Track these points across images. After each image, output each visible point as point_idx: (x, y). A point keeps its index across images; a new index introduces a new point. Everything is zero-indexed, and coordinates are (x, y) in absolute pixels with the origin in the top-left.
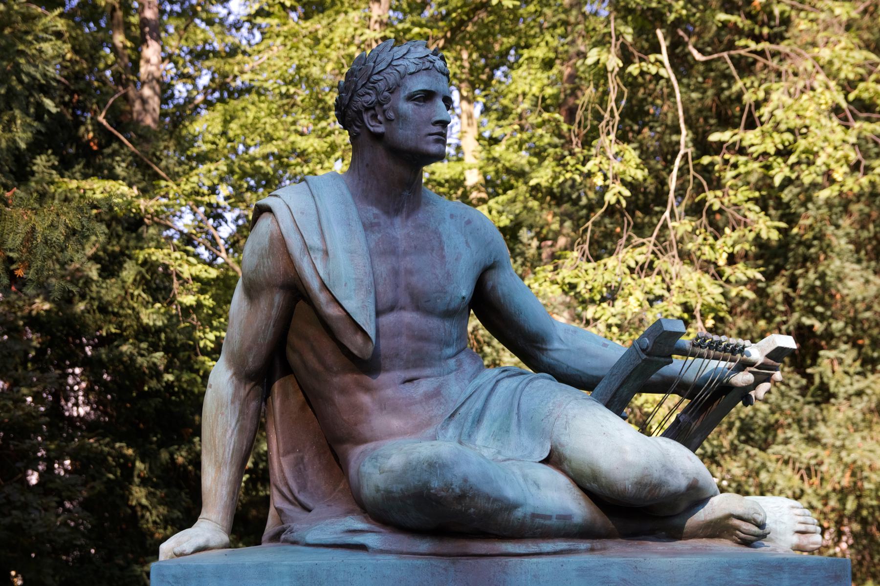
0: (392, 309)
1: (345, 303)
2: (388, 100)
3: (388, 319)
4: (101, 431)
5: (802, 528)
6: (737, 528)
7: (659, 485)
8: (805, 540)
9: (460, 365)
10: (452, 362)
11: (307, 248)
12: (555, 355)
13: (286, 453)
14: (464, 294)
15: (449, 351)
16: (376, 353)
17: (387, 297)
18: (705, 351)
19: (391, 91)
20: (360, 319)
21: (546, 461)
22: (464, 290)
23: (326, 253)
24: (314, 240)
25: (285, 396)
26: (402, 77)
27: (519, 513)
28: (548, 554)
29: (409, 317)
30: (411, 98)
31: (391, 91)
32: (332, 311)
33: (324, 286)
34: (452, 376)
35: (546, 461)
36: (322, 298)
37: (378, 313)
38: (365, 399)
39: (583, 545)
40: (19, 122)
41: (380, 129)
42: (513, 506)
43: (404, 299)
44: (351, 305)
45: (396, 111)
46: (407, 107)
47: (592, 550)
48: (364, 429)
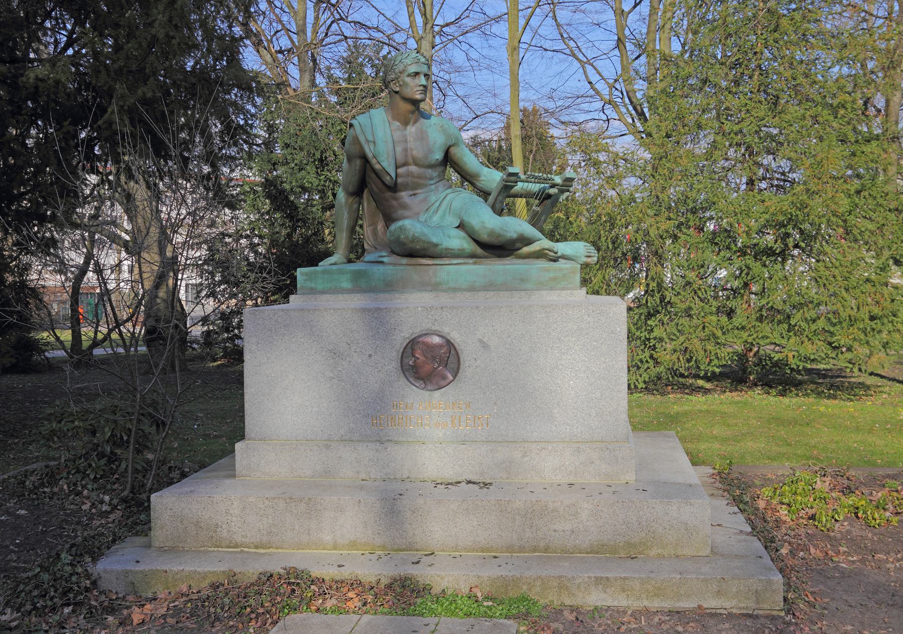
0: (405, 164)
1: (382, 164)
2: (399, 77)
3: (400, 171)
4: (543, 218)
5: (589, 254)
6: (547, 254)
7: (499, 236)
8: (589, 260)
9: (437, 188)
10: (433, 187)
11: (368, 141)
12: (483, 182)
13: (370, 226)
14: (437, 157)
15: (432, 182)
16: (396, 183)
17: (401, 159)
18: (533, 180)
19: (401, 73)
20: (388, 170)
21: (458, 227)
22: (439, 156)
23: (374, 142)
24: (370, 138)
25: (369, 201)
26: (405, 67)
27: (440, 247)
28: (457, 264)
29: (413, 169)
30: (409, 75)
31: (401, 73)
32: (377, 167)
33: (374, 157)
34: (432, 193)
35: (458, 227)
36: (374, 161)
37: (397, 167)
38: (394, 203)
39: (471, 261)
40: (153, 472)
41: (398, 89)
42: (436, 245)
43: (411, 160)
44: (385, 164)
45: (403, 82)
46: (408, 80)
47: (475, 263)
48: (394, 216)
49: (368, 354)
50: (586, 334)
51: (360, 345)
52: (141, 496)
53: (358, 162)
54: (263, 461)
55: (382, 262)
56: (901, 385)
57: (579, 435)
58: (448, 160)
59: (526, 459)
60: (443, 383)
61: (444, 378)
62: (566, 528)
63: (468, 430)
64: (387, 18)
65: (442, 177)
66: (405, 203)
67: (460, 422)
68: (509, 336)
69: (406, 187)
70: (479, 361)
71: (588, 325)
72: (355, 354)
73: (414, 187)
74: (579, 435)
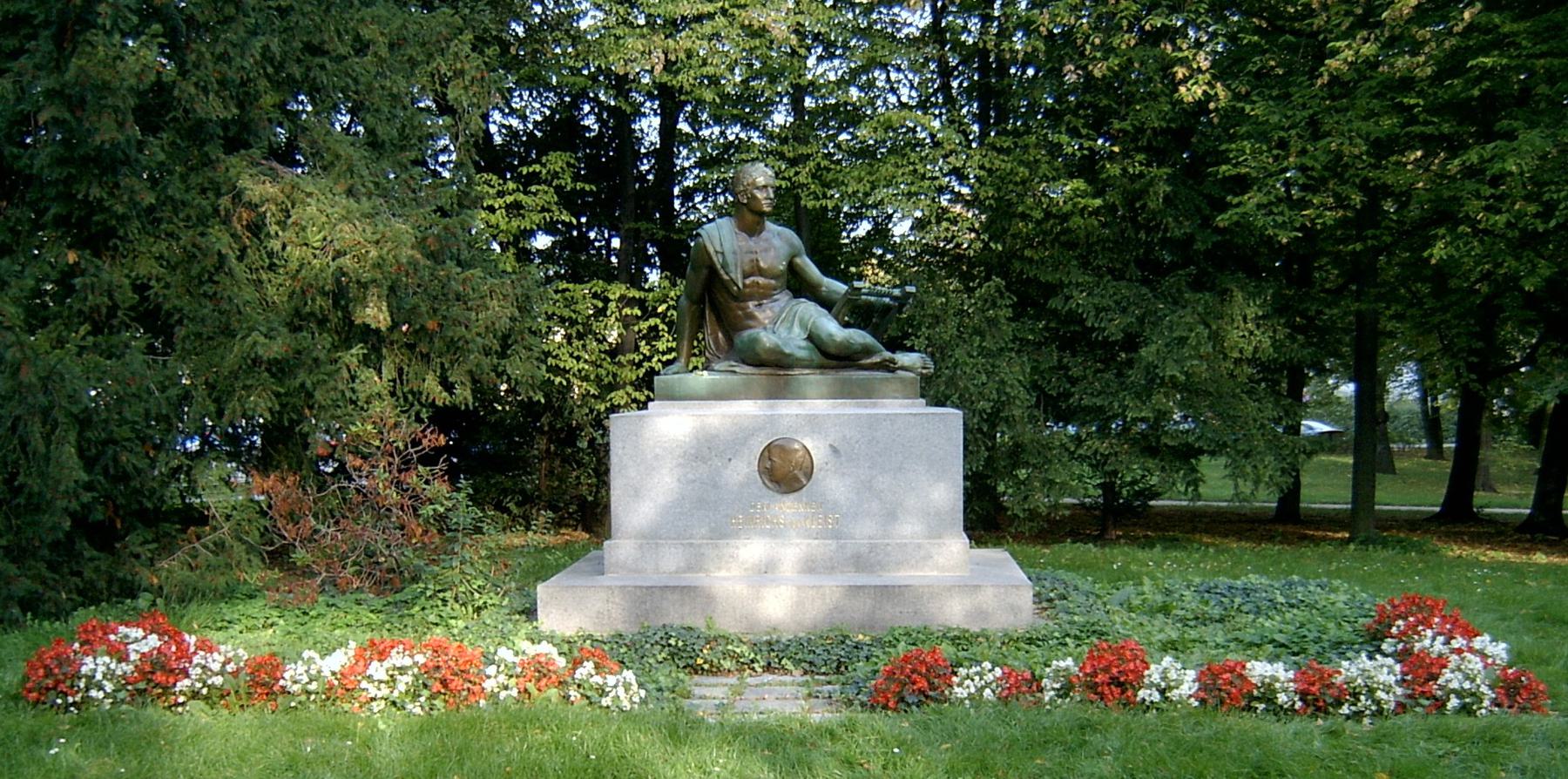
11: (717, 252)
23: (723, 253)
24: (719, 249)
55: (734, 372)
60: (797, 485)
73: (764, 295)
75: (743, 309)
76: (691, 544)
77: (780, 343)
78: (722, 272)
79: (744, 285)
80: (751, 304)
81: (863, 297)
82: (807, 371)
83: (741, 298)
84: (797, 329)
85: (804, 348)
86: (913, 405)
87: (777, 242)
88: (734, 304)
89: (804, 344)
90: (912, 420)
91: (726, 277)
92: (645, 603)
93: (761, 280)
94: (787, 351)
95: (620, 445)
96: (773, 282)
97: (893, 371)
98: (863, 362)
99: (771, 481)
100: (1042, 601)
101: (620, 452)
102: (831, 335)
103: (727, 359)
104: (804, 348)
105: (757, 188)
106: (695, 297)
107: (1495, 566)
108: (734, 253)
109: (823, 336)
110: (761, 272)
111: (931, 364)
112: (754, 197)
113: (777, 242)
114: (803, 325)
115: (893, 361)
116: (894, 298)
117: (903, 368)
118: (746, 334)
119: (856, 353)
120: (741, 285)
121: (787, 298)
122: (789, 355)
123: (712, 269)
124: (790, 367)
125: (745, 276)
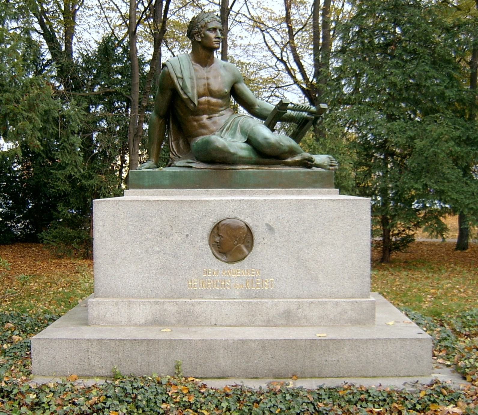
11: (177, 77)
23: (182, 79)
24: (179, 75)
44: (190, 95)
45: (204, 34)
49: (186, 234)
50: (342, 220)
51: (180, 227)
52: (435, 207)
53: (169, 94)
54: (108, 313)
55: (191, 167)
56: (236, 2)
57: (336, 293)
58: (234, 92)
59: (300, 310)
60: (240, 256)
61: (241, 251)
62: (334, 359)
63: (257, 290)
64: (265, 42)
65: (228, 105)
66: (204, 123)
67: (252, 284)
68: (288, 222)
69: (204, 112)
70: (266, 240)
71: (343, 214)
72: (176, 234)
73: (211, 110)
74: (336, 293)
75: (197, 121)
76: (157, 302)
77: (226, 144)
78: (181, 92)
79: (199, 103)
80: (205, 117)
81: (289, 112)
82: (247, 167)
83: (197, 112)
84: (238, 134)
85: (244, 149)
86: (329, 193)
87: (223, 72)
88: (191, 117)
89: (245, 145)
90: (331, 204)
91: (185, 97)
92: (118, 353)
93: (213, 100)
94: (232, 150)
95: (101, 223)
96: (220, 101)
97: (310, 167)
98: (289, 160)
99: (220, 252)
100: (87, 60)
101: (101, 229)
102: (266, 139)
103: (186, 158)
104: (244, 149)
105: (209, 30)
106: (162, 113)
107: (304, 173)
108: (191, 78)
109: (260, 139)
110: (211, 93)
111: (335, 162)
112: (207, 37)
113: (223, 72)
114: (244, 132)
115: (311, 160)
116: (311, 113)
117: (317, 166)
118: (199, 139)
119: (285, 153)
120: (196, 103)
121: (230, 113)
122: (233, 154)
123: (175, 92)
124: (234, 163)
125: (200, 96)
